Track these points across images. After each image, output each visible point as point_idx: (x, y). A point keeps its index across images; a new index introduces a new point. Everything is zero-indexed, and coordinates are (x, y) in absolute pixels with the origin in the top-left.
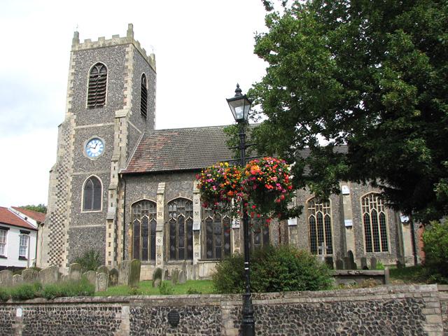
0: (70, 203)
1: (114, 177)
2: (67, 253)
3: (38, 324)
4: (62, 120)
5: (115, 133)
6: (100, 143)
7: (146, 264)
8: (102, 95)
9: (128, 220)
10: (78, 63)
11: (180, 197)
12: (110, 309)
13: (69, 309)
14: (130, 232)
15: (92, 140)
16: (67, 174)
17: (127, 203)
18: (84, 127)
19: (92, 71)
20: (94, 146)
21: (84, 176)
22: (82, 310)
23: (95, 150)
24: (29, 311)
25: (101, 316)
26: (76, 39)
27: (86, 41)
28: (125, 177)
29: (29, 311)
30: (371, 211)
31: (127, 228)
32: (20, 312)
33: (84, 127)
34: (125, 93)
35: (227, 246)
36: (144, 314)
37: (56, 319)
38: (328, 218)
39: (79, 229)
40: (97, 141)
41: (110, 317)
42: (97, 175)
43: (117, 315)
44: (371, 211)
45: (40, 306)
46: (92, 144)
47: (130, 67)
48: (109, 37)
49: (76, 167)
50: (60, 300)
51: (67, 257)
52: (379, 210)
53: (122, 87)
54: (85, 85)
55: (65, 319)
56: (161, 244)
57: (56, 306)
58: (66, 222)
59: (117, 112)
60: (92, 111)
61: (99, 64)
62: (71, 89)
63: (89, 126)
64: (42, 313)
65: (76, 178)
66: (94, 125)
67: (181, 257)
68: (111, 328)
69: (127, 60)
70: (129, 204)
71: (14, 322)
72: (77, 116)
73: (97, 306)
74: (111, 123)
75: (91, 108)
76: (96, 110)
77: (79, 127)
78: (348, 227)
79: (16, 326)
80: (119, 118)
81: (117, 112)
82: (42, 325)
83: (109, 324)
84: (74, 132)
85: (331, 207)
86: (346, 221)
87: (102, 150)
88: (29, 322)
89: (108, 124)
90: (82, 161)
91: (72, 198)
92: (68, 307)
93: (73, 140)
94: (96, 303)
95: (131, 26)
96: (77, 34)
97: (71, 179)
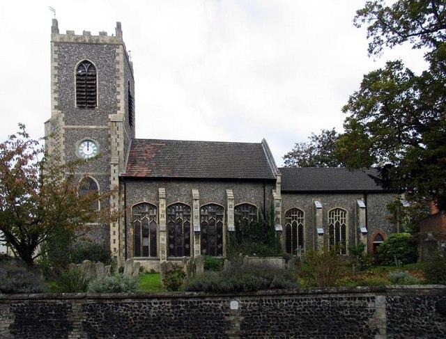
1: (114, 179)
3: (261, 315)
4: (49, 117)
5: (112, 137)
6: (93, 145)
7: (148, 259)
8: (93, 96)
11: (179, 202)
12: (360, 298)
13: (305, 299)
14: (131, 231)
15: (86, 141)
17: (128, 204)
22: (322, 301)
24: (249, 303)
25: (348, 305)
26: (55, 29)
27: (68, 32)
29: (249, 303)
30: (335, 222)
31: (128, 227)
32: (234, 305)
34: (118, 97)
35: (187, 246)
36: (405, 303)
37: (287, 310)
38: (301, 227)
40: (90, 143)
41: (360, 307)
42: (92, 176)
43: (370, 305)
44: (335, 222)
45: (263, 299)
47: (122, 71)
48: (95, 33)
52: (342, 222)
53: (114, 90)
54: (71, 81)
55: (300, 310)
57: (287, 298)
59: (110, 116)
60: (83, 111)
61: (86, 62)
62: (56, 84)
63: (80, 126)
64: (267, 305)
66: (86, 127)
68: (362, 317)
69: (118, 63)
70: (130, 205)
71: (226, 315)
72: (66, 115)
73: (343, 296)
74: (104, 127)
75: (81, 108)
77: (69, 126)
78: (320, 234)
79: (232, 318)
80: (115, 122)
81: (110, 116)
82: (268, 317)
83: (359, 313)
84: (63, 131)
85: (304, 217)
86: (318, 229)
87: (95, 152)
88: (249, 318)
89: (101, 127)
92: (303, 298)
93: (63, 139)
94: (342, 293)
95: (119, 26)
96: (55, 22)
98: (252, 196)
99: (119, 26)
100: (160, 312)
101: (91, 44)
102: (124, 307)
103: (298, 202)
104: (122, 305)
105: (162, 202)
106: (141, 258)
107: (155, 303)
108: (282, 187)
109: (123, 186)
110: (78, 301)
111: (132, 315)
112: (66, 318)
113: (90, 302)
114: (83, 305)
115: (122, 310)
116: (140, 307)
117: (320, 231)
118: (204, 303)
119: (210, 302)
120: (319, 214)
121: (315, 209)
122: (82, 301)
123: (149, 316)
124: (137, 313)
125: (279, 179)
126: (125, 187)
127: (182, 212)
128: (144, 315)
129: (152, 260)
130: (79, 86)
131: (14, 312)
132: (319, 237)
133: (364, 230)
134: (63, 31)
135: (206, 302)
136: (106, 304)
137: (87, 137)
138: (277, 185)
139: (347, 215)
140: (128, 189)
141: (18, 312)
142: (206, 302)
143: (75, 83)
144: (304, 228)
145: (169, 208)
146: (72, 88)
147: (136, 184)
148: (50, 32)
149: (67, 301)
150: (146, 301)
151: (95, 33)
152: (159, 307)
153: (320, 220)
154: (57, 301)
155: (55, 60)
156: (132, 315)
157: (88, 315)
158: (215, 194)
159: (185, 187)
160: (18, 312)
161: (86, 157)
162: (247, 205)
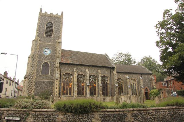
0: (36, 71)
2: (34, 90)
6: (49, 50)
9: (61, 79)
10: (42, 20)
14: (62, 84)
15: (47, 48)
16: (35, 59)
18: (43, 43)
19: (47, 24)
20: (47, 51)
21: (42, 61)
23: (47, 52)
26: (41, 11)
27: (45, 12)
28: (61, 64)
33: (43, 43)
39: (39, 81)
46: (46, 50)
49: (39, 57)
50: (102, 110)
51: (34, 92)
56: (58, 90)
58: (34, 78)
60: (47, 38)
61: (50, 22)
65: (39, 61)
67: (67, 94)
74: (54, 44)
76: (49, 38)
81: (57, 41)
89: (53, 44)
90: (42, 55)
91: (37, 69)
93: (38, 47)
95: (62, 12)
96: (172, 9)
97: (37, 62)
98: (107, 73)
99: (62, 12)
100: (164, 115)
101: (52, 17)
102: (149, 114)
103: (121, 76)
104: (148, 113)
105: (75, 73)
106: (65, 95)
107: (162, 112)
108: (117, 70)
109: (60, 66)
110: (130, 112)
111: (153, 118)
112: (125, 120)
113: (135, 112)
114: (132, 114)
115: (148, 116)
116: (156, 114)
117: (129, 87)
118: (180, 111)
119: (183, 110)
120: (128, 80)
121: (127, 79)
122: (131, 112)
123: (160, 117)
124: (155, 116)
125: (116, 67)
126: (61, 66)
127: (82, 78)
128: (158, 117)
129: (69, 96)
130: (52, 29)
131: (101, 117)
132: (129, 89)
133: (143, 87)
134: (43, 12)
135: (181, 110)
136: (142, 113)
137: (47, 47)
138: (115, 69)
139: (136, 81)
140: (62, 67)
141: (103, 118)
142: (181, 110)
143: (45, 28)
144: (123, 86)
145: (102, 77)
146: (44, 30)
147: (65, 66)
148: (64, 17)
149: (125, 112)
150: (158, 111)
151: (54, 14)
152: (163, 113)
153: (129, 83)
154: (121, 112)
155: (39, 20)
156: (153, 118)
157: (134, 118)
158: (94, 71)
159: (83, 68)
160: (103, 118)
161: (46, 54)
162: (81, 75)
